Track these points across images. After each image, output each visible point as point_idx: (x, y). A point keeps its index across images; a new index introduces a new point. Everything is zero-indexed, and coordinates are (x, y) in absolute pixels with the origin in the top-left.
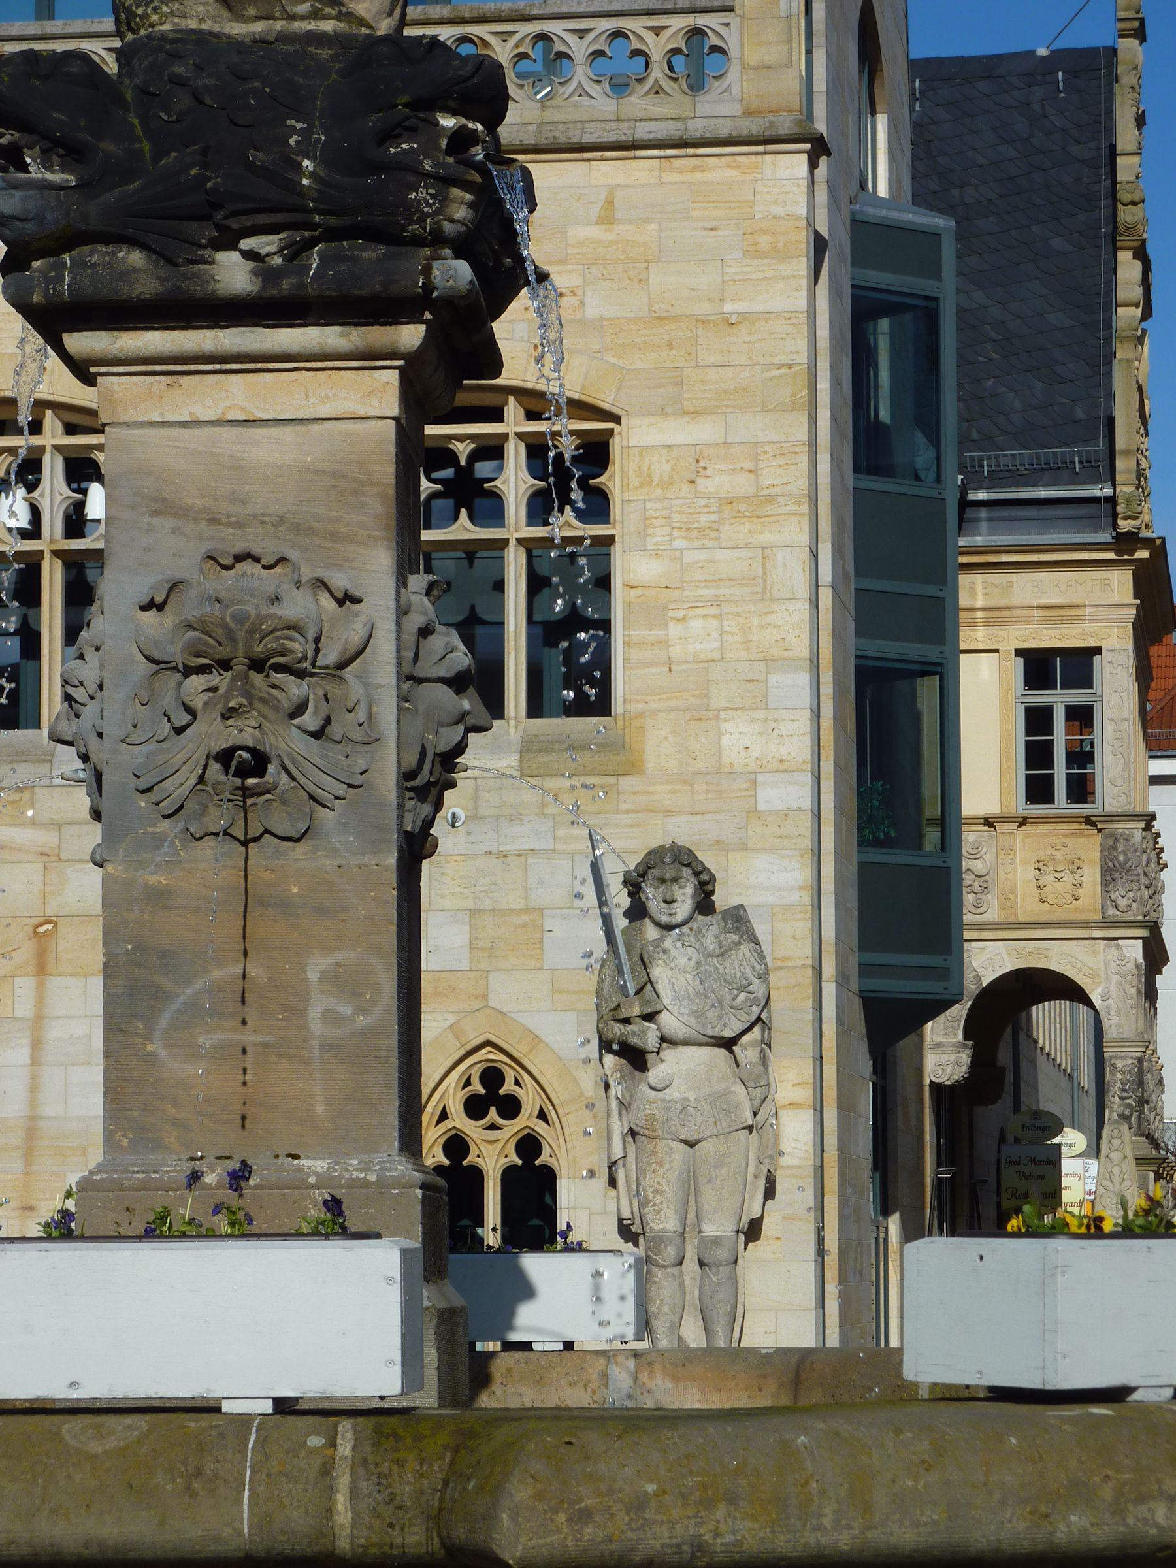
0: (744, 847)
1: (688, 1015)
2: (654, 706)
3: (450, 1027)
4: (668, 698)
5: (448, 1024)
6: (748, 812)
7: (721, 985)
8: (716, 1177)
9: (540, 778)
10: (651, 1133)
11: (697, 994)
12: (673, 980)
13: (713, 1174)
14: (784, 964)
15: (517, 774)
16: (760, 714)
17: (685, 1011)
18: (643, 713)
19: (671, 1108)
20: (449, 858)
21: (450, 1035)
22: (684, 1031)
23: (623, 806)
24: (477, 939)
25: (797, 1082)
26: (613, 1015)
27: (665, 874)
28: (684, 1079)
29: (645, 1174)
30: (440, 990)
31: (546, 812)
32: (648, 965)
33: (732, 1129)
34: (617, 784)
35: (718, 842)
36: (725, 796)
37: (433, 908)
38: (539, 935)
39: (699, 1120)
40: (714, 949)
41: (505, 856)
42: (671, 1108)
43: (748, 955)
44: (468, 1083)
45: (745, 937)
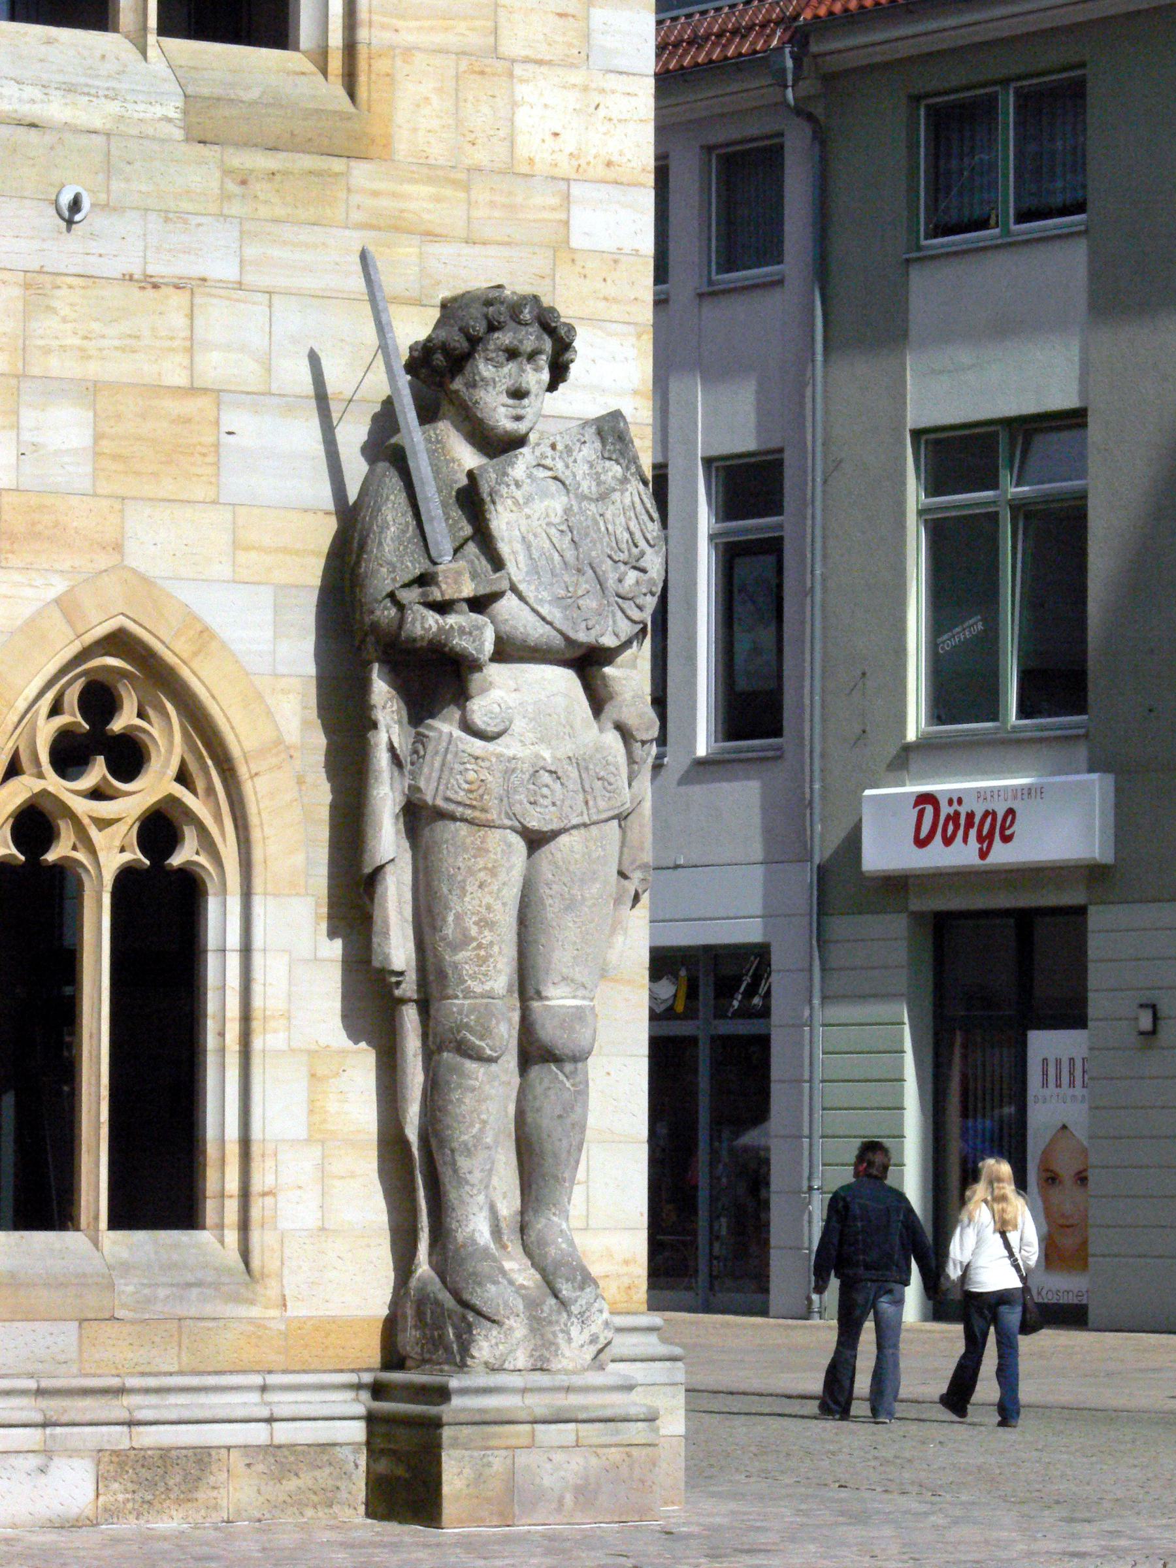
1: (550, 602)
2: (408, 38)
3: (57, 601)
4: (432, 29)
5: (52, 593)
10: (477, 814)
15: (179, 134)
16: (577, 77)
18: (392, 48)
19: (514, 770)
20: (59, 280)
21: (57, 615)
22: (541, 631)
26: (424, 595)
28: (531, 720)
29: (463, 889)
30: (39, 528)
31: (226, 212)
34: (346, 174)
35: (636, 299)
36: (520, 216)
38: (211, 439)
42: (514, 770)
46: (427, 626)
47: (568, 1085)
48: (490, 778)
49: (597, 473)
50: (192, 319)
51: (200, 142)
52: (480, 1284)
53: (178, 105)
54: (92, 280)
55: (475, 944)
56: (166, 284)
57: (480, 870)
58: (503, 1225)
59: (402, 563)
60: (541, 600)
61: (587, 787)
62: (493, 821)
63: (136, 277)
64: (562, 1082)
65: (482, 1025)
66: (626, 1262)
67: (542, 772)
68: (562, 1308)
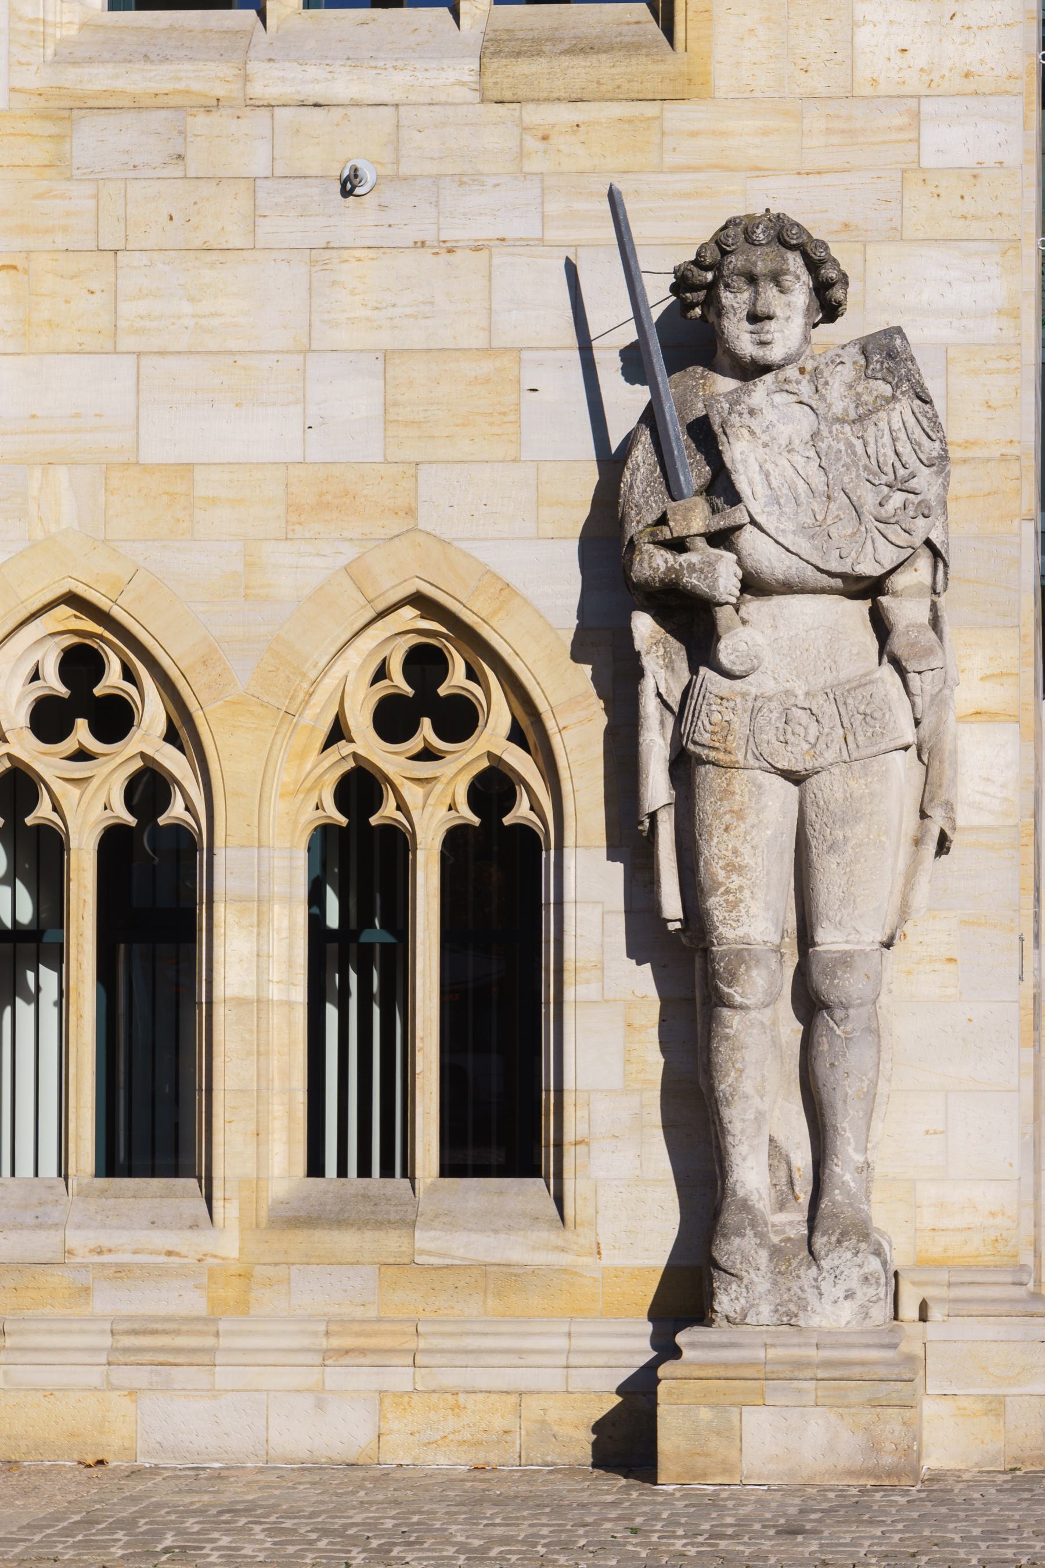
0: (896, 235)
1: (794, 533)
5: (343, 560)
6: (904, 171)
7: (858, 476)
9: (516, 106)
12: (768, 466)
13: (839, 834)
17: (790, 526)
20: (345, 254)
22: (787, 563)
23: (670, 159)
24: (396, 404)
25: (989, 673)
26: (652, 534)
27: (755, 264)
31: (526, 169)
33: (875, 750)
37: (314, 347)
40: (846, 410)
41: (450, 251)
44: (381, 674)
45: (905, 387)
46: (654, 565)
47: (838, 1032)
48: (735, 719)
49: (858, 394)
50: (490, 280)
51: (496, 103)
52: (724, 1236)
53: (472, 67)
54: (382, 250)
55: (722, 889)
56: (463, 248)
57: (725, 813)
58: (796, 1176)
59: (647, 503)
60: (783, 531)
61: (847, 724)
62: (737, 762)
63: (428, 243)
64: (832, 1028)
65: (730, 972)
66: (993, 1214)
67: (794, 709)
68: (813, 1262)
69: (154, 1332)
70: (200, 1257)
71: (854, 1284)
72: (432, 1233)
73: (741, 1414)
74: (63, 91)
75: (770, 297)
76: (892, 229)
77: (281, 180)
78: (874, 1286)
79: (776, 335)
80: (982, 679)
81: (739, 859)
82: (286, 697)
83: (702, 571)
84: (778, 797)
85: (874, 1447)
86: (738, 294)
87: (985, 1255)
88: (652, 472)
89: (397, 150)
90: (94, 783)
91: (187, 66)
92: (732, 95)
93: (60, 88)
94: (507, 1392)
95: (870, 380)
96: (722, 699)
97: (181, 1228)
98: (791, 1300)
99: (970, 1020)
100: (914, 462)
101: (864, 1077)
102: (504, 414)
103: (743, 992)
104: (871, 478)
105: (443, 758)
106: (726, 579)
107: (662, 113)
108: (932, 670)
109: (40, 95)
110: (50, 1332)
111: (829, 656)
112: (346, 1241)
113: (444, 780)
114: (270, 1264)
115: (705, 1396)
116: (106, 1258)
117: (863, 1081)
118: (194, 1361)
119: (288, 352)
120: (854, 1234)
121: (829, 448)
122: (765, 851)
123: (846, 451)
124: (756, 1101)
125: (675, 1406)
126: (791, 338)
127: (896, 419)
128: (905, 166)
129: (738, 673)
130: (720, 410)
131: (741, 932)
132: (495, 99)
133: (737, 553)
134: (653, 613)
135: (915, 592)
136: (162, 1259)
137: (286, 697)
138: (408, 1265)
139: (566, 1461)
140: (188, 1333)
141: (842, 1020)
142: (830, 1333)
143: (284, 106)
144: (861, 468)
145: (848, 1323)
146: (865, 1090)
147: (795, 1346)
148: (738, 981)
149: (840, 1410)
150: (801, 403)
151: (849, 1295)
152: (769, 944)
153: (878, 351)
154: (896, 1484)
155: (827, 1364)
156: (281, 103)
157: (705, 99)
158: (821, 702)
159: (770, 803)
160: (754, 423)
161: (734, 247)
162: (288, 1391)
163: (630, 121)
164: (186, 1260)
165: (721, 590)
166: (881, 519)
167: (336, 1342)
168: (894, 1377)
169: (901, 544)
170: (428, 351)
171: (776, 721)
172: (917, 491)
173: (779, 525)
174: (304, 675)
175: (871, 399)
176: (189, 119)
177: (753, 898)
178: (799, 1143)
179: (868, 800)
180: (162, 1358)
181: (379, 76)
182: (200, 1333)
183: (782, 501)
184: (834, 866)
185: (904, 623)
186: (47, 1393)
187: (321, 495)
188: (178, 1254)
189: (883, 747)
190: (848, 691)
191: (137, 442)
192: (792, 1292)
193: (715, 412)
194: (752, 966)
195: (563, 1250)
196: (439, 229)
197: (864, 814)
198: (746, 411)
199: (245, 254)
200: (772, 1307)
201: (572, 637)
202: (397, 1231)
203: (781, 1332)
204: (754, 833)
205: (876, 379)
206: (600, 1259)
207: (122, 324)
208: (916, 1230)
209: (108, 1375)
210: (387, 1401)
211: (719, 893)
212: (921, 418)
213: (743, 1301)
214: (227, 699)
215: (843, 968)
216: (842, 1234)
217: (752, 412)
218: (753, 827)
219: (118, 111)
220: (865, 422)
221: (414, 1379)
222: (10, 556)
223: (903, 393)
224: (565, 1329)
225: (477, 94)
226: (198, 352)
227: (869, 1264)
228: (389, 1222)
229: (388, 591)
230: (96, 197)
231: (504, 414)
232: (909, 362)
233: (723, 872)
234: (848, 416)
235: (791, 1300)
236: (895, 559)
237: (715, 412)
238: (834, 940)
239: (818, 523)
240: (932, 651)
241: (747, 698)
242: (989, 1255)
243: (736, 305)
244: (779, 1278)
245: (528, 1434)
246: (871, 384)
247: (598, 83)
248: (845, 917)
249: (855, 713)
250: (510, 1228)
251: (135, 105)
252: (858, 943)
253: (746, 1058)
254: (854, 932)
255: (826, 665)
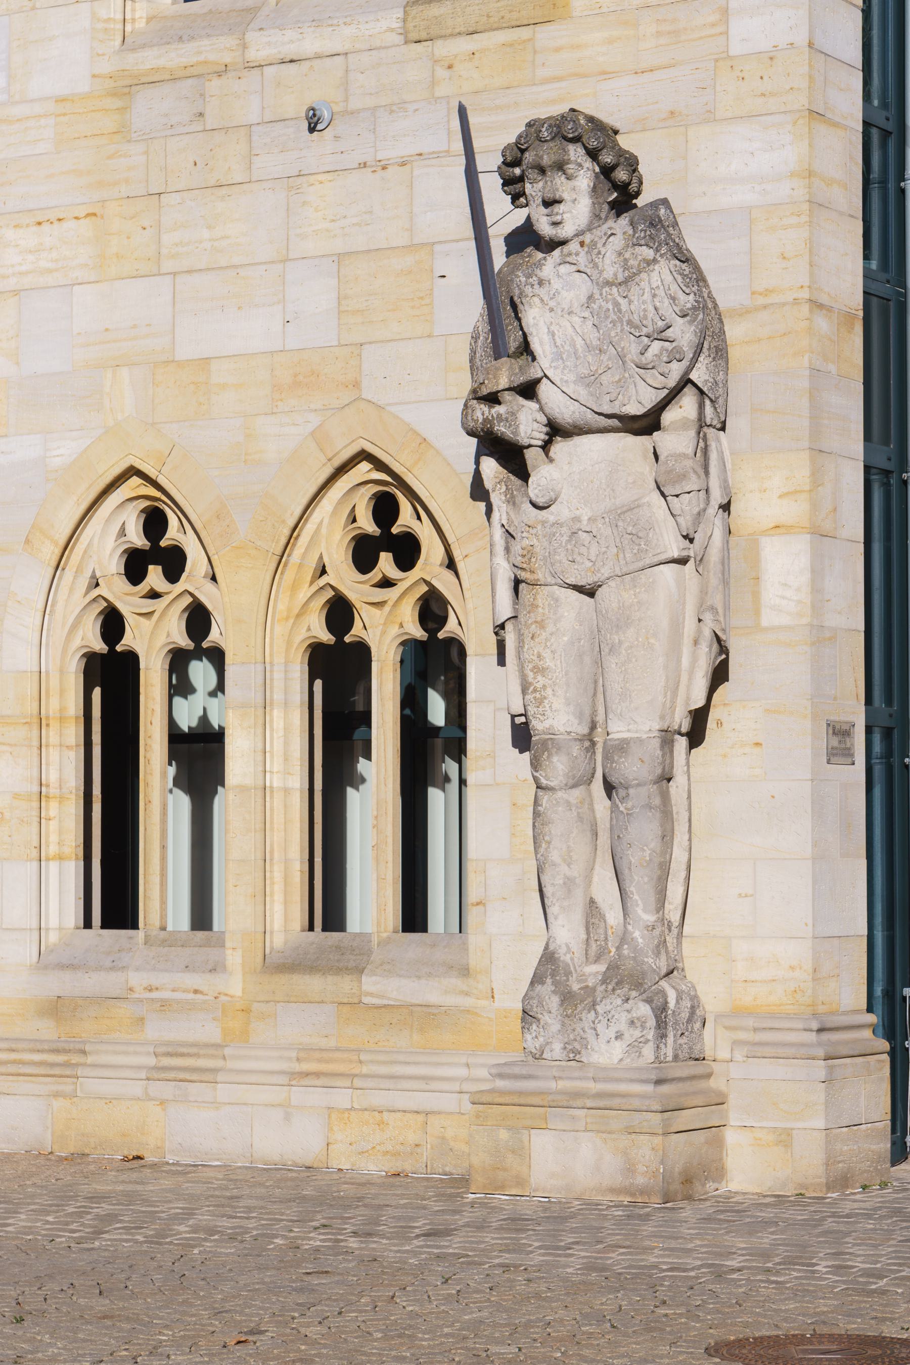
0: (710, 117)
1: (575, 382)
3: (312, 433)
6: (716, 60)
7: (622, 330)
8: (620, 642)
11: (588, 347)
12: (554, 328)
13: (616, 639)
14: (768, 300)
15: (400, 39)
17: (571, 377)
20: (312, 178)
22: (572, 408)
27: (541, 158)
31: (437, 94)
32: (520, 307)
33: (640, 564)
35: (791, 89)
39: (594, 550)
40: (615, 275)
41: (384, 168)
43: (668, 278)
46: (475, 418)
47: (622, 809)
51: (416, 42)
53: (399, 16)
54: (336, 173)
55: (531, 688)
57: (532, 624)
60: (566, 382)
62: (538, 580)
63: (368, 164)
66: (792, 968)
67: (580, 532)
69: (182, 1055)
70: (216, 995)
71: (623, 1026)
72: (374, 978)
73: (530, 1135)
74: (126, 73)
75: (559, 184)
76: (708, 111)
77: (268, 125)
78: (639, 1029)
79: (565, 216)
80: (780, 497)
81: (542, 662)
82: (273, 541)
83: (507, 421)
84: (573, 608)
85: (630, 1169)
86: (534, 184)
87: (787, 1004)
88: (487, 339)
89: (346, 90)
90: (156, 616)
91: (206, 42)
92: (586, 13)
93: (123, 70)
94: (417, 1112)
95: (636, 247)
96: (529, 527)
97: (204, 972)
98: (575, 1040)
99: (773, 797)
100: (671, 314)
101: (645, 848)
102: (422, 298)
103: (546, 775)
104: (632, 330)
105: (396, 584)
106: (526, 426)
107: (534, 35)
108: (689, 493)
109: (111, 77)
110: (116, 1053)
111: (608, 486)
112: (314, 984)
113: (390, 603)
114: (263, 1002)
115: (504, 1119)
116: (154, 995)
117: (644, 850)
118: (203, 1079)
119: (273, 262)
120: (628, 983)
121: (600, 308)
122: (563, 654)
123: (613, 309)
124: (564, 868)
125: (482, 1127)
126: (579, 216)
127: (655, 279)
128: (716, 56)
129: (541, 505)
130: (519, 283)
131: (547, 724)
132: (415, 40)
133: (538, 401)
134: (497, 457)
135: (683, 424)
136: (191, 996)
137: (273, 541)
138: (356, 1004)
139: (460, 1172)
140: (205, 1056)
141: (623, 798)
142: (605, 1069)
143: (270, 64)
144: (625, 323)
145: (621, 1060)
146: (648, 858)
147: (577, 1079)
148: (541, 766)
149: (604, 1135)
150: (579, 271)
151: (619, 1036)
152: (573, 734)
153: (642, 222)
154: (647, 1201)
155: (600, 1095)
156: (268, 63)
157: (565, 19)
158: (600, 525)
159: (566, 614)
160: (542, 292)
161: (526, 145)
162: (266, 1105)
163: (511, 45)
164: (206, 998)
165: (523, 435)
166: (640, 366)
167: (305, 1067)
168: (645, 1108)
169: (657, 386)
170: (369, 251)
171: (566, 544)
172: (670, 339)
173: (563, 377)
174: (283, 522)
175: (635, 263)
176: (207, 83)
177: (554, 695)
178: (612, 905)
179: (637, 608)
180: (182, 1076)
181: (335, 32)
182: (213, 1056)
183: (564, 356)
184: (613, 666)
185: (665, 454)
186: (107, 1101)
187: (296, 375)
188: (201, 993)
189: (648, 561)
190: (619, 515)
191: (174, 343)
192: (576, 1033)
193: (515, 286)
194: (554, 753)
195: (467, 994)
196: (376, 151)
197: (633, 620)
198: (536, 282)
199: (244, 186)
200: (562, 1045)
201: (471, 480)
202: (350, 976)
203: (570, 1066)
204: (552, 640)
205: (641, 245)
206: (493, 1002)
207: (164, 251)
208: (732, 981)
209: (146, 1088)
210: (333, 1116)
211: (530, 691)
212: (676, 276)
213: (541, 1039)
214: (233, 545)
215: (620, 754)
216: (617, 984)
217: (541, 283)
218: (552, 634)
219: (161, 84)
220: (629, 283)
221: (352, 1099)
222: (93, 440)
223: (662, 256)
224: (464, 1060)
225: (402, 37)
226: (213, 269)
227: (638, 1009)
228: (347, 969)
229: (340, 451)
230: (146, 153)
231: (422, 298)
232: (671, 228)
233: (532, 673)
234: (616, 279)
235: (575, 1040)
236: (654, 399)
237: (515, 286)
238: (619, 729)
239: (592, 373)
240: (685, 476)
241: (546, 525)
242: (790, 1004)
243: (534, 194)
244: (567, 1021)
245: (432, 1148)
246: (637, 250)
247: (488, 16)
248: (624, 709)
249: (624, 534)
250: (430, 975)
251: (172, 77)
252: (637, 732)
253: (552, 832)
254: (632, 722)
255: (606, 493)
